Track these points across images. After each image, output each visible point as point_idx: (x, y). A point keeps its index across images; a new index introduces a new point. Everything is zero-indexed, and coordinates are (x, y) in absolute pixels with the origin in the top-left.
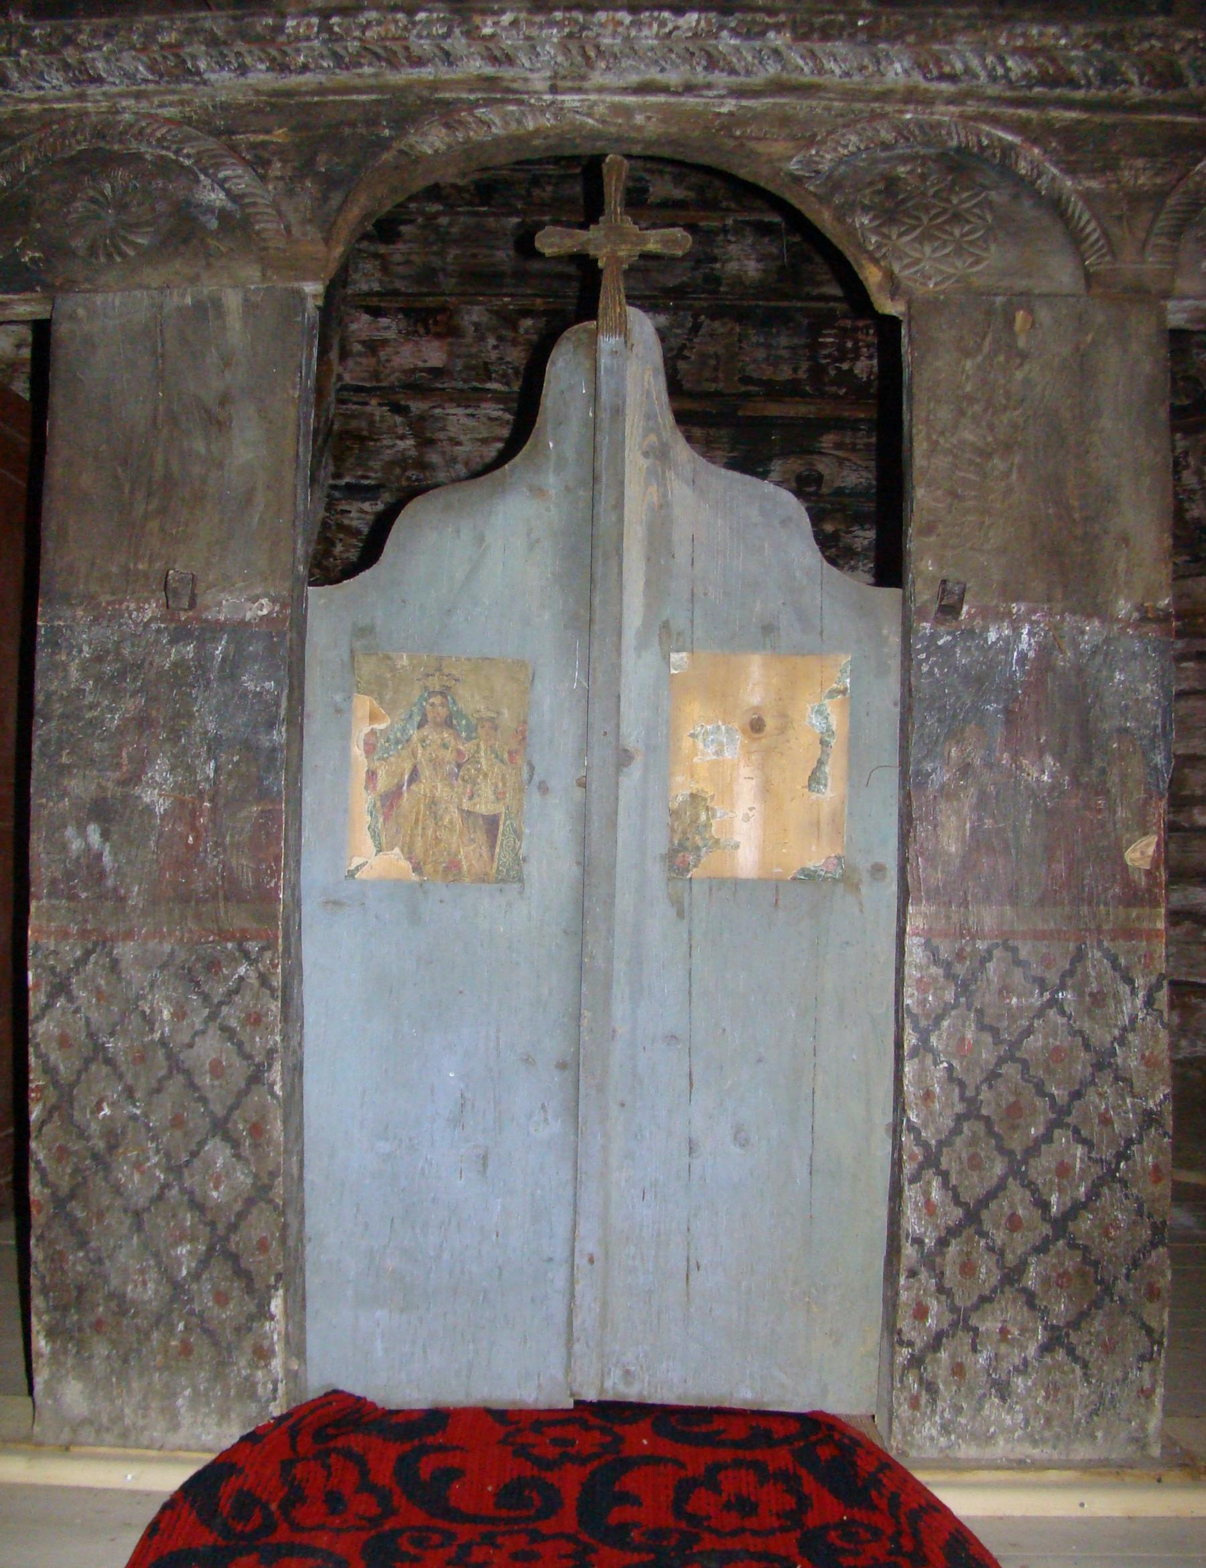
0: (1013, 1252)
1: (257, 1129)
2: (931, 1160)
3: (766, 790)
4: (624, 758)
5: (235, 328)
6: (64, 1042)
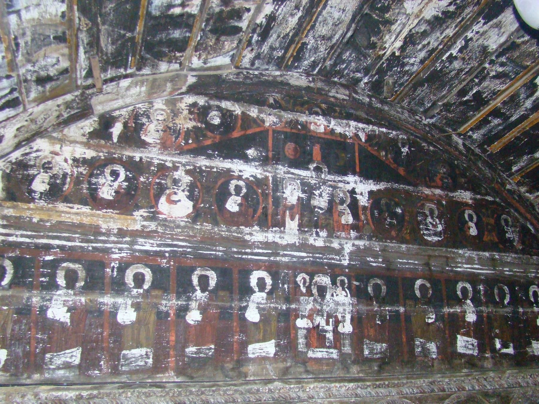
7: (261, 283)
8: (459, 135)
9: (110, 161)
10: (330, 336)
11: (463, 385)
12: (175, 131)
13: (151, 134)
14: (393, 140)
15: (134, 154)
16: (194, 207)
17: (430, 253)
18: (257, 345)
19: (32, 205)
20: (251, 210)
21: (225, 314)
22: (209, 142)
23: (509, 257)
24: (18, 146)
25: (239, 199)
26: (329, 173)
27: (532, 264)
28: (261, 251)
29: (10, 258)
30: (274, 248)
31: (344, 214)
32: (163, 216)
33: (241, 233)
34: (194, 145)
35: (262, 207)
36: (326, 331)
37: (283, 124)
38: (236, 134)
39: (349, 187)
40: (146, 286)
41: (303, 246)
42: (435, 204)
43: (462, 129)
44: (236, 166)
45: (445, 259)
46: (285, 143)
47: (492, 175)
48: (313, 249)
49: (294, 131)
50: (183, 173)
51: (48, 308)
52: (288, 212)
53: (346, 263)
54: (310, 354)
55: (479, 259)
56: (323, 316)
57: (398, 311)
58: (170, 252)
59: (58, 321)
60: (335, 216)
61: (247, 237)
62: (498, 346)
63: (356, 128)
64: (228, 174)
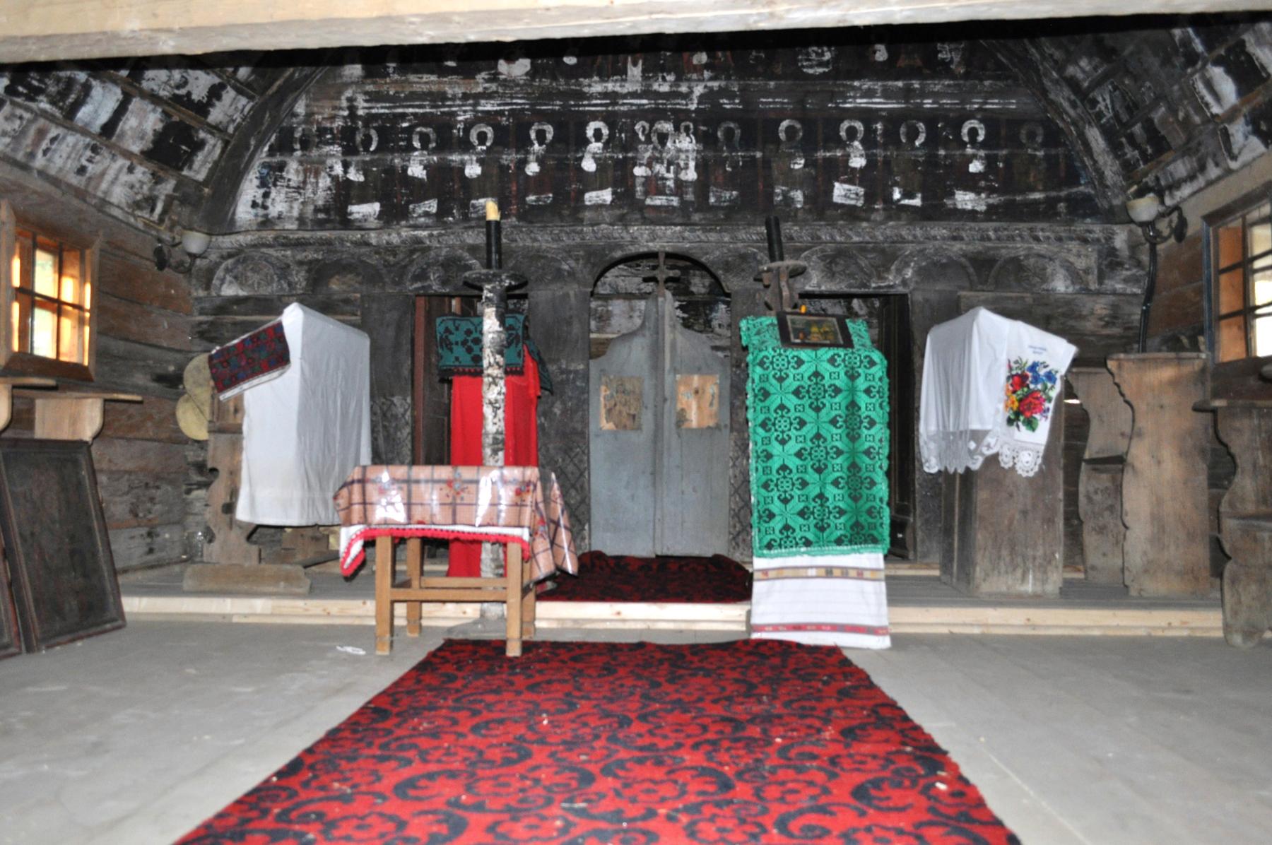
0: (170, 77)
1: (582, 487)
3: (699, 408)
4: (665, 400)
5: (573, 300)
29: (375, 128)
30: (613, 97)
40: (488, 144)
53: (693, 107)
54: (648, 202)
61: (586, 89)
62: (897, 195)
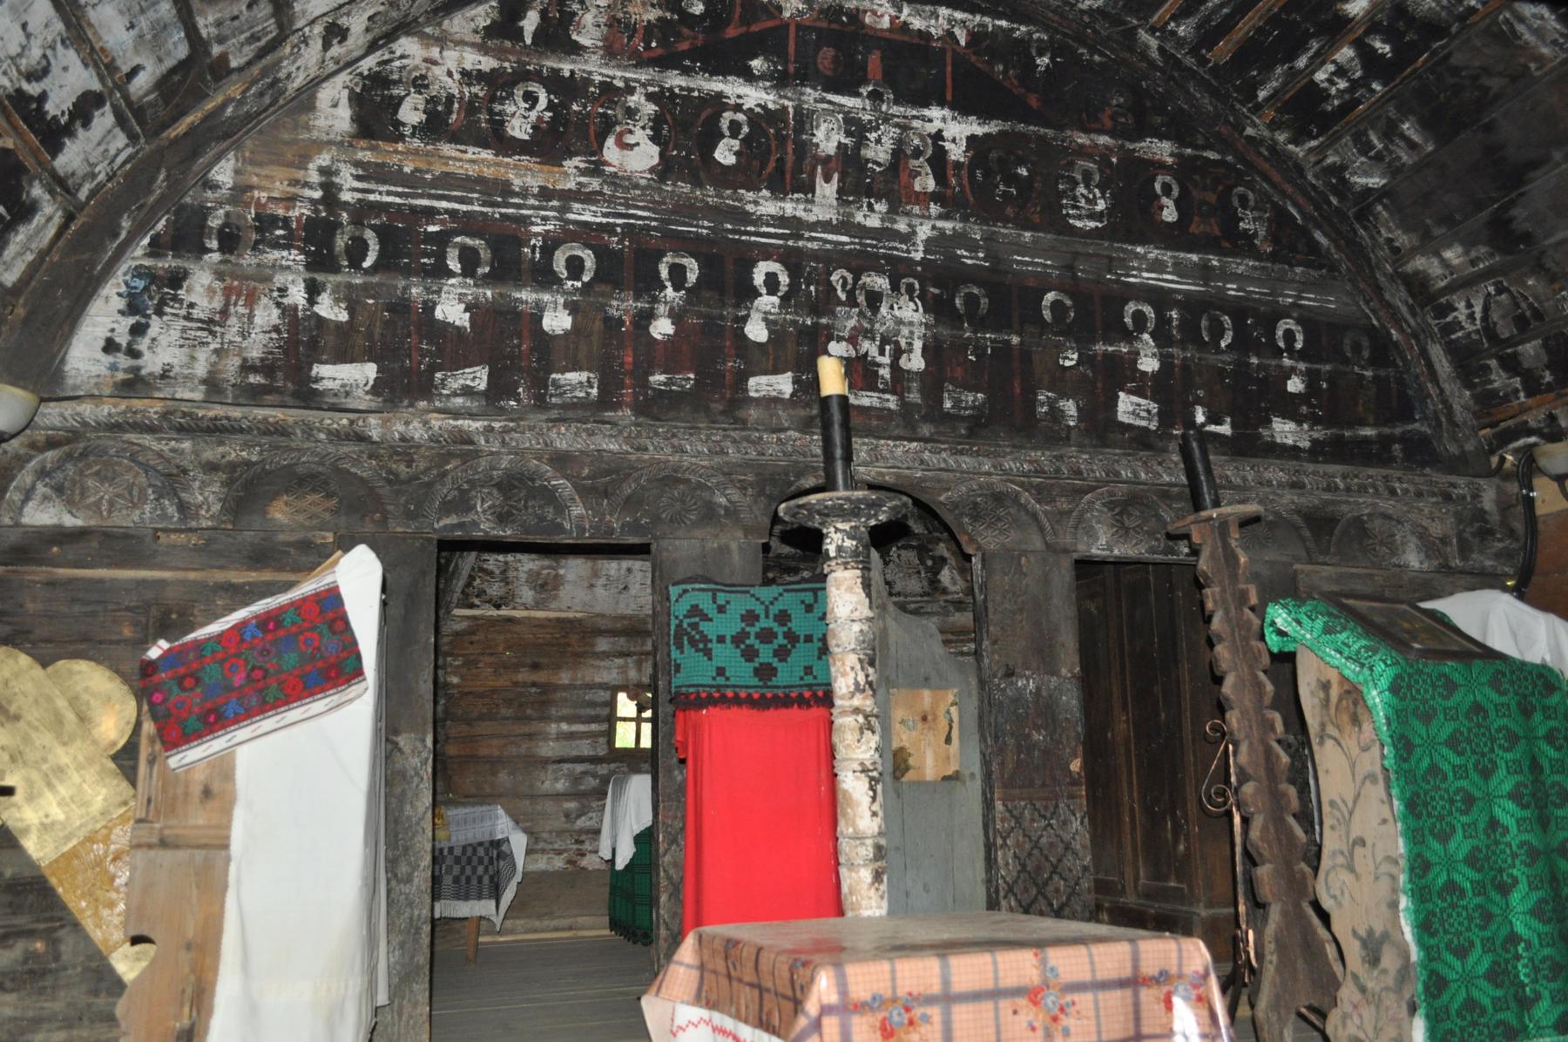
2: (1010, 890)
6: (675, 864)
7: (772, 282)
8: (1152, 30)
9: (522, 76)
10: (885, 372)
11: (1116, 467)
12: (627, 26)
13: (588, 34)
14: (1020, 41)
15: (561, 66)
16: (662, 155)
17: (1080, 248)
18: (763, 379)
19: (400, 147)
20: (756, 163)
21: (712, 328)
22: (685, 46)
23: (1241, 266)
24: (372, 48)
25: (736, 144)
26: (896, 102)
27: (1293, 281)
28: (772, 230)
31: (919, 174)
32: (612, 169)
33: (740, 200)
34: (660, 51)
35: (777, 156)
36: (879, 365)
37: (815, 14)
38: (732, 32)
39: (931, 128)
41: (845, 226)
42: (1095, 162)
43: (1156, 18)
44: (732, 88)
45: (1106, 261)
46: (818, 48)
47: (1215, 107)
48: (862, 231)
49: (834, 26)
50: (643, 99)
51: (435, 304)
52: (819, 169)
53: (918, 256)
55: (1176, 264)
56: (873, 339)
57: (1008, 342)
58: (623, 226)
59: (452, 325)
60: (904, 177)
61: (750, 208)
63: (949, 21)
64: (717, 102)
